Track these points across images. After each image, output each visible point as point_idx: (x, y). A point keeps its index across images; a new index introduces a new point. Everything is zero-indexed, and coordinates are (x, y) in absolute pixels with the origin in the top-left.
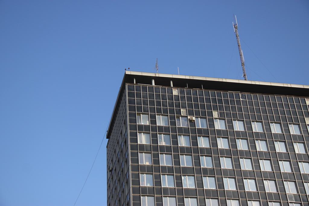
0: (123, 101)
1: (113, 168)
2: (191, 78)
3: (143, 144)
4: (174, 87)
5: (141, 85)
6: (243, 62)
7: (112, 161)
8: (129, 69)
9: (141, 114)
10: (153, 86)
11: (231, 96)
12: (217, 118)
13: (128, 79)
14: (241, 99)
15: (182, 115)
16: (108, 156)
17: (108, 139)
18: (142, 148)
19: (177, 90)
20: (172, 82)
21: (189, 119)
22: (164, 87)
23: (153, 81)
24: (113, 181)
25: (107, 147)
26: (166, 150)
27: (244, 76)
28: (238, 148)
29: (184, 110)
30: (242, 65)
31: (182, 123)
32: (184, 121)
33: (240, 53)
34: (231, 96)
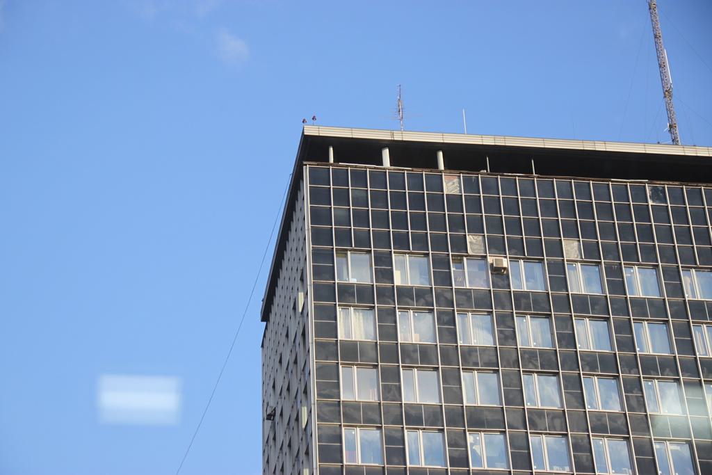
0: (297, 215)
1: (275, 409)
2: (500, 142)
3: (353, 340)
4: (448, 171)
5: (350, 167)
6: (669, 86)
7: (274, 387)
8: (314, 118)
9: (349, 253)
10: (384, 169)
11: (622, 194)
12: (576, 261)
13: (312, 148)
14: (650, 203)
15: (470, 252)
16: (264, 374)
17: (265, 323)
18: (351, 352)
19: (456, 180)
20: (331, 150)
21: (492, 264)
22: (417, 171)
23: (386, 154)
24: (275, 445)
25: (262, 346)
26: (421, 356)
27: (670, 131)
28: (638, 349)
29: (476, 237)
30: (665, 97)
31: (469, 277)
32: (476, 270)
33: (658, 57)
34: (603, 194)
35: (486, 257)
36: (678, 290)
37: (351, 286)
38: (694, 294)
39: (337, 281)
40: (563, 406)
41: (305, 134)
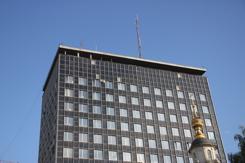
0: (56, 66)
1: (46, 112)
2: (105, 54)
5: (70, 56)
7: (45, 106)
8: (62, 44)
9: (68, 76)
12: (120, 83)
13: (61, 51)
14: (137, 71)
15: (96, 78)
16: (43, 103)
17: (44, 92)
18: (67, 99)
19: (94, 61)
20: (91, 55)
21: (101, 82)
22: (85, 58)
23: (78, 54)
25: (43, 97)
30: (139, 48)
31: (96, 84)
33: (138, 39)
35: (100, 80)
36: (129, 89)
37: (69, 84)
38: (145, 92)
39: (65, 82)
40: (115, 115)
41: (60, 47)
